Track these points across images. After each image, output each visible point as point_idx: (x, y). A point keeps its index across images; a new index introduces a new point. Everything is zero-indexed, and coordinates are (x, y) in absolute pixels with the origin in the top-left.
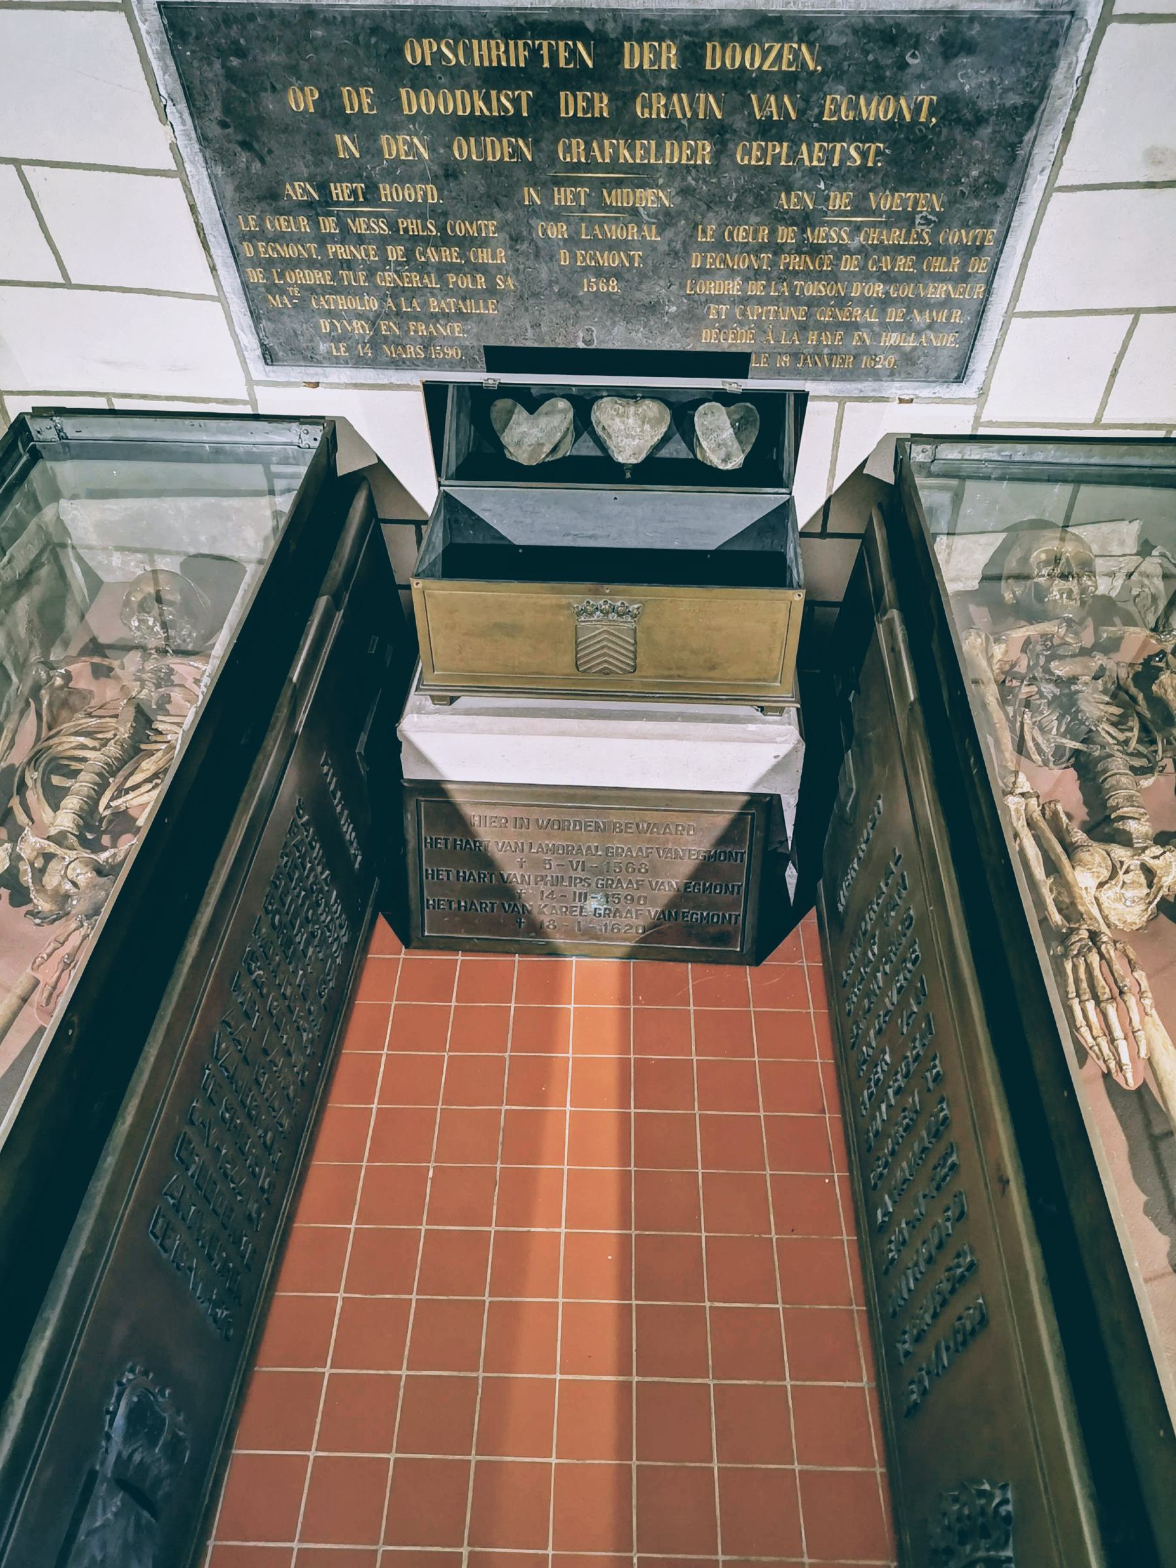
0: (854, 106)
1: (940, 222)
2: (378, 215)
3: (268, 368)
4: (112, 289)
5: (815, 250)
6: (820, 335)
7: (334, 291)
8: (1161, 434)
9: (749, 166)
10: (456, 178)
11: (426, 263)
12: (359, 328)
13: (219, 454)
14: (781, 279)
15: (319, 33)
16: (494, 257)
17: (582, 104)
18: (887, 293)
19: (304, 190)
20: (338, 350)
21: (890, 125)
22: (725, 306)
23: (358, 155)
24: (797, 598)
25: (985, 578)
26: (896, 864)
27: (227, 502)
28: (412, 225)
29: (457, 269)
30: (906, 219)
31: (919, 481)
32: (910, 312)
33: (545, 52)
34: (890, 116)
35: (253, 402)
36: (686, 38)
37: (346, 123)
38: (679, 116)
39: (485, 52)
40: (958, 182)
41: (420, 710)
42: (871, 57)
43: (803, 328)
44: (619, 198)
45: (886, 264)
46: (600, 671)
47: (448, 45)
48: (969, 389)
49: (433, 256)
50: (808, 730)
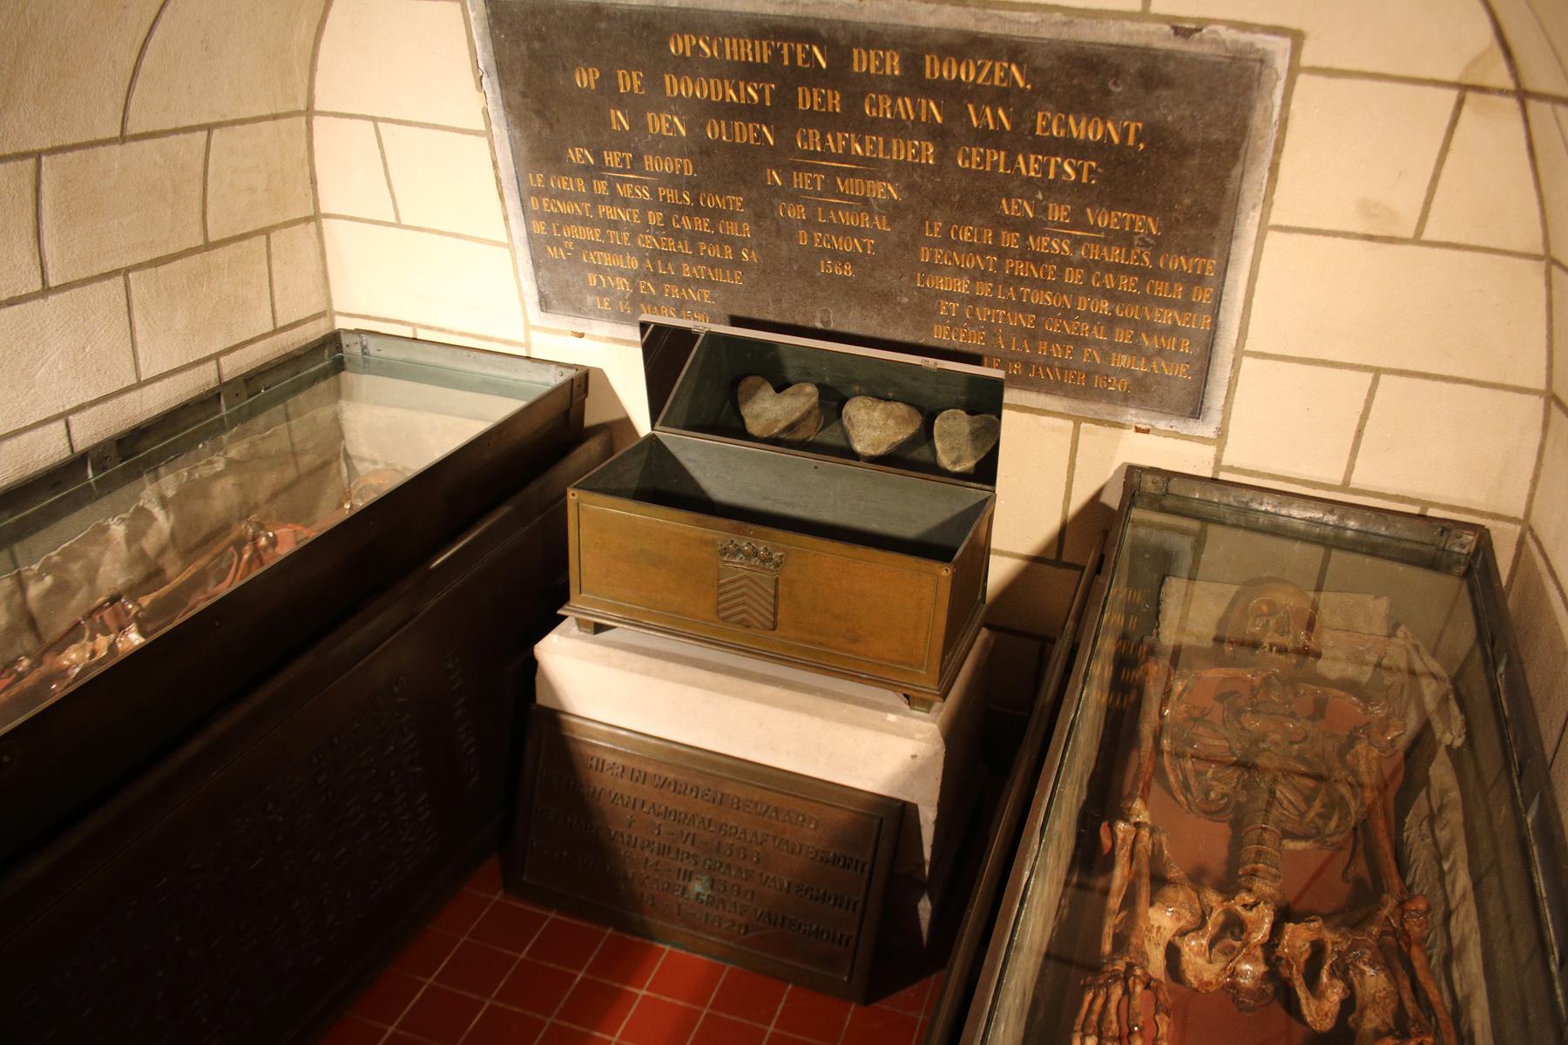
0: (1064, 124)
1: (1158, 246)
2: (642, 183)
5: (1039, 259)
6: (1049, 347)
7: (602, 248)
8: (1415, 510)
11: (680, 230)
12: (622, 284)
15: (603, 25)
17: (817, 99)
18: (1113, 312)
22: (955, 299)
24: (944, 573)
29: (707, 238)
32: (1136, 336)
33: (785, 51)
34: (1099, 137)
35: (527, 346)
37: (621, 101)
39: (735, 48)
42: (1075, 81)
43: (1032, 336)
46: (739, 622)
48: (1207, 429)
49: (686, 223)
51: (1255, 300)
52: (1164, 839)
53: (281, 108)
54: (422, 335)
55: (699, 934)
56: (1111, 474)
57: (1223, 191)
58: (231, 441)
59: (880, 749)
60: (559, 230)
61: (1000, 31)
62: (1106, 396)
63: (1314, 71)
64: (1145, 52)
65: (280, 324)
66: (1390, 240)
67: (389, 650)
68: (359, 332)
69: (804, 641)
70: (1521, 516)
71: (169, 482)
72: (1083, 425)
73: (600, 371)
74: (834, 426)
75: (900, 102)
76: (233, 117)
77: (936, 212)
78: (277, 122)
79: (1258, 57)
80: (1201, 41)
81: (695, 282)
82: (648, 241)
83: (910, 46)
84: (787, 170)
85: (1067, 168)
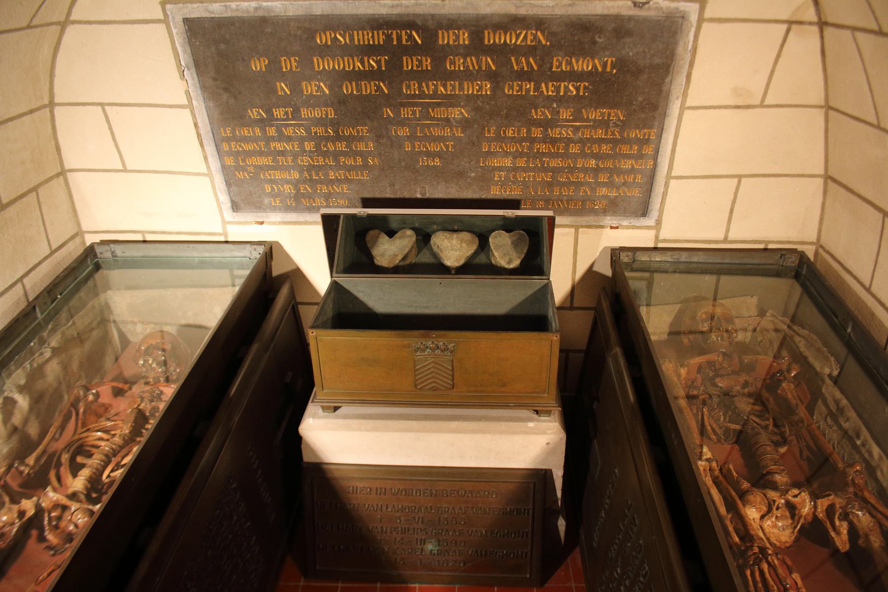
1: (623, 126)
2: (299, 125)
3: (235, 214)
4: (149, 172)
5: (554, 141)
8: (762, 246)
9: (512, 95)
10: (345, 104)
12: (288, 189)
13: (203, 264)
14: (535, 157)
16: (367, 147)
17: (416, 63)
18: (597, 165)
19: (258, 112)
20: (275, 202)
21: (590, 72)
22: (503, 170)
23: (289, 93)
24: (555, 338)
25: (670, 334)
26: (629, 510)
27: (204, 291)
28: (320, 131)
29: (344, 154)
30: (604, 124)
31: (628, 274)
32: (611, 176)
33: (394, 36)
35: (225, 234)
36: (474, 28)
37: (283, 77)
38: (471, 68)
40: (631, 104)
41: (314, 416)
42: (576, 38)
43: (550, 185)
44: (440, 113)
45: (595, 149)
46: (430, 389)
47: (340, 34)
48: (650, 221)
49: (331, 147)
50: (570, 424)
51: (677, 148)
52: (731, 467)
53: (34, 106)
54: (149, 238)
55: (435, 573)
56: (598, 254)
57: (660, 91)
58: (49, 336)
59: (529, 443)
60: (244, 161)
61: (531, 13)
62: (593, 212)
63: (712, 20)
64: (617, 18)
65: (54, 248)
66: (748, 107)
67: (218, 455)
68: (103, 243)
69: (472, 392)
70: (815, 241)
71: (19, 376)
72: (581, 230)
73: (277, 243)
74: (425, 251)
75: (468, 59)
76: (7, 117)
77: (492, 121)
78: (33, 115)
79: (681, 15)
80: (649, 9)
81: (339, 181)
82: (305, 161)
83: (475, 26)
84: (396, 108)
85: (571, 88)
